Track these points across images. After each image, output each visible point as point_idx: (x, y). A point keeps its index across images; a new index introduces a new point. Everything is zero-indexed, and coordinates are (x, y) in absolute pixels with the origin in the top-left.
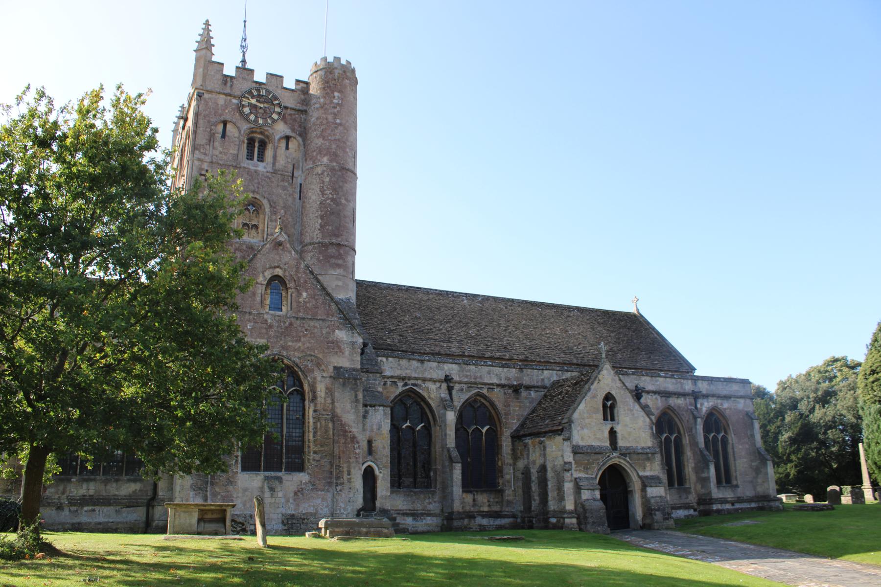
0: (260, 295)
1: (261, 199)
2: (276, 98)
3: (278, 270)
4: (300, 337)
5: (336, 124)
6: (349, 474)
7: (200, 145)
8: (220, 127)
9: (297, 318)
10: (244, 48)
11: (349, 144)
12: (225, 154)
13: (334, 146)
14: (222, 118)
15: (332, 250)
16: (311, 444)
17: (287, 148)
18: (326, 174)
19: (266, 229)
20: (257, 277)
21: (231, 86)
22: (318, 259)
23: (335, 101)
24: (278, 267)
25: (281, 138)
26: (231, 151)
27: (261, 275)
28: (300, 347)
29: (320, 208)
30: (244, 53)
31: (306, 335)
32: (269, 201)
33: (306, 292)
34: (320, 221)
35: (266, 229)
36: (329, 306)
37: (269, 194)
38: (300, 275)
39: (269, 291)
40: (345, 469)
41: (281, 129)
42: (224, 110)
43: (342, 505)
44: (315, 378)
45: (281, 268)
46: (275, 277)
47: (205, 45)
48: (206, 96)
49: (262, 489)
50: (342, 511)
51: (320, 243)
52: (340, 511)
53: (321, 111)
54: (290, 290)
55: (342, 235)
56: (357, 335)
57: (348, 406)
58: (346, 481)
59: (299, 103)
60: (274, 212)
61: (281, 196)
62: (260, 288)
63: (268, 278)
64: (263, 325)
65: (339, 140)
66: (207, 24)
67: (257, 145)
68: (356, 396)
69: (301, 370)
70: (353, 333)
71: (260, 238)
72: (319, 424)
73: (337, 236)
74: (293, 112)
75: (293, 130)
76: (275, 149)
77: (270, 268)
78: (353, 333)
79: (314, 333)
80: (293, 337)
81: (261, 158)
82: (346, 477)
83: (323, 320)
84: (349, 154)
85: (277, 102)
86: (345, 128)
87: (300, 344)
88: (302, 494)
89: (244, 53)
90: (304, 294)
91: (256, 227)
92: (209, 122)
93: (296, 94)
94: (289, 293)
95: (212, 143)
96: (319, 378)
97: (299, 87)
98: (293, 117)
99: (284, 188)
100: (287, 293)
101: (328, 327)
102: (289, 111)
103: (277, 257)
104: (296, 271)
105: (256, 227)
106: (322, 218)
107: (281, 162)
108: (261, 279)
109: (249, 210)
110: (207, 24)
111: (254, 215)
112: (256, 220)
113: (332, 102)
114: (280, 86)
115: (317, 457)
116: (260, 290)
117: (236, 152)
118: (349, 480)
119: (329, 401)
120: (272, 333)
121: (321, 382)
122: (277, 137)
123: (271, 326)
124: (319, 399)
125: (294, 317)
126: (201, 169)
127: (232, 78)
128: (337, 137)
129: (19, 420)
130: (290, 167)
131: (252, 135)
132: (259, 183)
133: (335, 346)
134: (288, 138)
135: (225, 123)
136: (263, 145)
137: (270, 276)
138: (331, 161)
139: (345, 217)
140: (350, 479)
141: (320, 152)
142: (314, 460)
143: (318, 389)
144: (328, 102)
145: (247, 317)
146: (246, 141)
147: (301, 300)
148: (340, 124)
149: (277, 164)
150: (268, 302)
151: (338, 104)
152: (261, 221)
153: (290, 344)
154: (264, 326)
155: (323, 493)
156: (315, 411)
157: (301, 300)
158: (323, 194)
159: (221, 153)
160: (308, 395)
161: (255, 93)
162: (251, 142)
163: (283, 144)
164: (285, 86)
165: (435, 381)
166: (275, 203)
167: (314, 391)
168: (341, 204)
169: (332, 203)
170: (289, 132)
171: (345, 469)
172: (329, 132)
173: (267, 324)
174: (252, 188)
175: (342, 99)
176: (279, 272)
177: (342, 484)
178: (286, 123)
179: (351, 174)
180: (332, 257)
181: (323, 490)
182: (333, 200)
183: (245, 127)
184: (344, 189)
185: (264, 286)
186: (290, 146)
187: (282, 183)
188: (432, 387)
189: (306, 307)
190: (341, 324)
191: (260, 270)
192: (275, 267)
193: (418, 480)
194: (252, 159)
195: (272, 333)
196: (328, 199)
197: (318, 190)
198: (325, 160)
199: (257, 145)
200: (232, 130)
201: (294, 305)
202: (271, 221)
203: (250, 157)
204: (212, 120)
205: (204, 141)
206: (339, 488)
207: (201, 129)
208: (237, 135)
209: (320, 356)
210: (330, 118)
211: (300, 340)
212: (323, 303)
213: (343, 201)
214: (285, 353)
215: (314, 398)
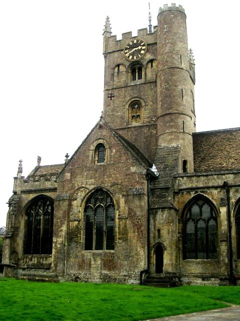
3: (100, 140)
8: (116, 69)
10: (150, 20)
13: (166, 57)
16: (117, 234)
17: (152, 66)
20: (90, 147)
25: (148, 62)
45: (101, 139)
47: (107, 32)
55: (172, 108)
63: (95, 146)
65: (168, 52)
66: (108, 18)
67: (137, 71)
69: (111, 194)
73: (169, 109)
81: (140, 77)
84: (176, 58)
91: (139, 116)
105: (139, 116)
107: (149, 75)
110: (108, 18)
115: (121, 241)
116: (91, 153)
134: (151, 61)
135: (118, 66)
136: (140, 70)
143: (121, 203)
150: (97, 159)
159: (117, 82)
160: (116, 207)
162: (133, 72)
163: (150, 65)
165: (216, 188)
167: (118, 203)
176: (101, 141)
183: (127, 64)
186: (154, 65)
188: (215, 192)
199: (137, 71)
202: (145, 111)
203: (134, 79)
208: (125, 70)
215: (119, 207)
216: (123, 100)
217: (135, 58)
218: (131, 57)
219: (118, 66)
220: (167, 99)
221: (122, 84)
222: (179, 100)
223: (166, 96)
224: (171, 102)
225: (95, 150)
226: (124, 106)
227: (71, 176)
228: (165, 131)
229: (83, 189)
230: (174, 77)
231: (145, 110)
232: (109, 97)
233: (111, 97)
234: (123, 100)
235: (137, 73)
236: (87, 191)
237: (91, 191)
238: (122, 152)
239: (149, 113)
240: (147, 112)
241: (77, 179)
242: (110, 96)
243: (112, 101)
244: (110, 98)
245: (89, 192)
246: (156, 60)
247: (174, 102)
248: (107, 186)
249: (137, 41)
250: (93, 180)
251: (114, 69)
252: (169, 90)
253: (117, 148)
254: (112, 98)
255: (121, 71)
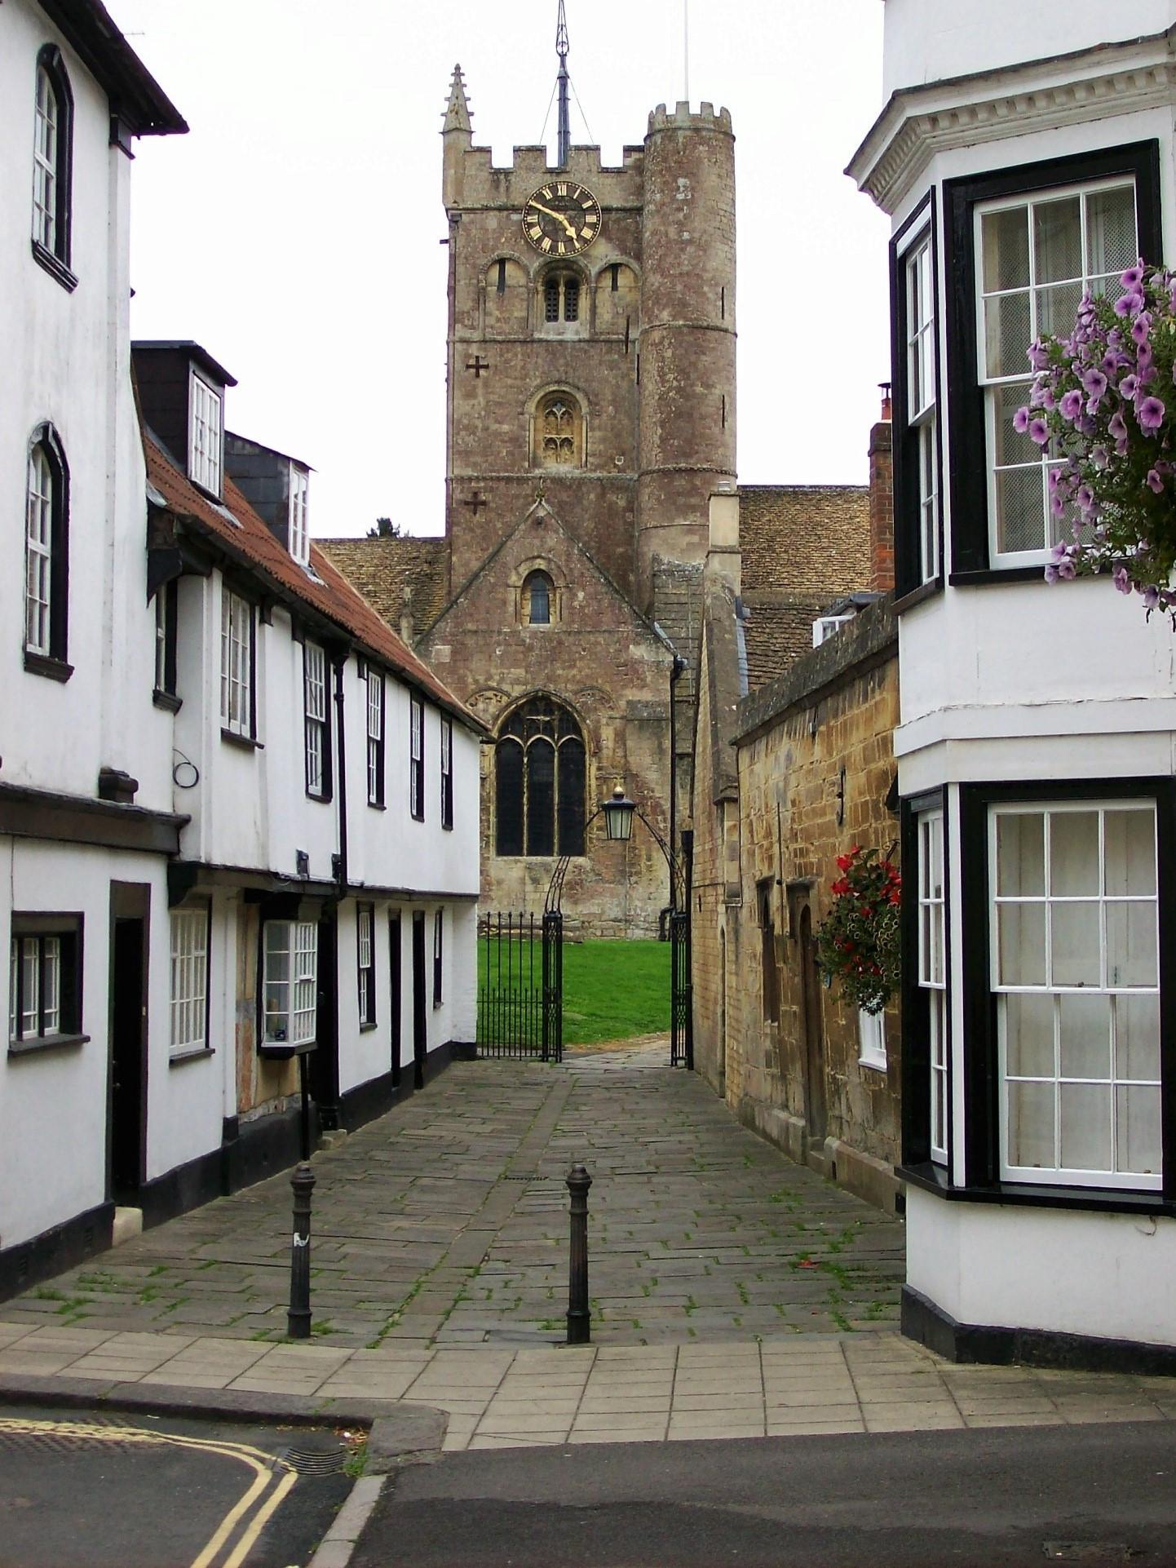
0: (513, 604)
1: (574, 392)
2: (586, 196)
3: (539, 561)
4: (575, 661)
5: (682, 242)
6: (649, 859)
7: (463, 313)
8: (494, 273)
9: (569, 633)
11: (707, 276)
12: (507, 320)
13: (679, 287)
14: (495, 256)
15: (681, 482)
17: (615, 287)
18: (666, 343)
19: (584, 445)
20: (507, 576)
21: (508, 188)
22: (658, 499)
23: (680, 197)
24: (539, 557)
26: (516, 314)
27: (514, 572)
28: (574, 676)
29: (659, 406)
30: (563, 56)
31: (584, 656)
32: (586, 395)
33: (584, 590)
34: (660, 431)
35: (584, 445)
36: (620, 608)
37: (586, 381)
38: (573, 566)
39: (528, 595)
40: (644, 852)
41: (604, 252)
42: (499, 238)
43: (639, 904)
44: (598, 721)
45: (543, 558)
46: (536, 574)
48: (465, 218)
49: (523, 882)
50: (639, 911)
51: (659, 470)
52: (635, 910)
53: (657, 220)
54: (558, 591)
56: (664, 650)
57: (648, 760)
58: (644, 870)
59: (633, 194)
60: (594, 414)
61: (607, 381)
62: (514, 592)
63: (524, 575)
64: (518, 648)
65: (688, 274)
66: (458, 72)
67: (562, 289)
68: (660, 744)
70: (658, 648)
71: (575, 462)
72: (605, 787)
73: (687, 455)
74: (620, 215)
75: (624, 251)
76: (594, 292)
77: (527, 560)
78: (658, 648)
79: (596, 654)
80: (564, 662)
81: (572, 316)
82: (643, 862)
83: (610, 632)
84: (710, 295)
85: (590, 203)
86: (699, 247)
87: (574, 672)
88: (581, 887)
89: (563, 56)
90: (581, 595)
92: (474, 266)
93: (626, 177)
94: (558, 595)
95: (482, 306)
96: (604, 721)
97: (630, 161)
98: (623, 224)
99: (612, 366)
100: (555, 595)
101: (618, 641)
102: (614, 215)
103: (537, 542)
104: (567, 561)
105: (567, 442)
106: (663, 424)
107: (605, 314)
108: (513, 579)
109: (555, 414)
110: (458, 72)
111: (565, 420)
112: (568, 429)
113: (674, 199)
114: (594, 169)
116: (512, 595)
117: (524, 314)
118: (649, 868)
119: (620, 753)
120: (532, 659)
121: (608, 724)
122: (594, 270)
123: (530, 648)
124: (605, 751)
125: (565, 632)
126: (468, 356)
127: (506, 172)
128: (685, 269)
129: (1071, 534)
130: (622, 322)
131: (552, 274)
132: (567, 365)
133: (631, 672)
134: (614, 268)
135: (502, 262)
136: (573, 286)
137: (527, 572)
138: (674, 318)
139: (703, 417)
140: (651, 866)
141: (657, 302)
142: (598, 839)
143: (604, 737)
144: (667, 200)
145: (495, 638)
146: (541, 288)
147: (576, 604)
148: (690, 242)
149: (597, 321)
150: (528, 610)
151: (685, 201)
152: (576, 430)
153: (560, 672)
154: (521, 648)
155: (612, 885)
156: (599, 769)
157: (576, 604)
158: (663, 381)
159: (498, 320)
160: (589, 747)
161: (549, 195)
162: (551, 286)
163: (607, 282)
164: (604, 164)
166: (596, 395)
167: (597, 740)
168: (694, 395)
169: (677, 397)
170: (615, 257)
171: (644, 852)
172: (670, 260)
173: (524, 645)
174: (556, 375)
175: (693, 189)
176: (541, 564)
177: (638, 873)
178: (609, 239)
179: (716, 334)
180: (679, 494)
181: (613, 883)
182: (679, 390)
183: (535, 264)
184: (700, 366)
185: (519, 590)
187: (607, 358)
189: (585, 614)
190: (637, 634)
191: (512, 565)
192: (535, 558)
193: (36, 1012)
194: (556, 318)
195: (532, 659)
196: (670, 389)
197: (656, 373)
198: (665, 315)
199: (562, 289)
200: (513, 274)
201: (565, 613)
202: (593, 429)
204: (478, 262)
205: (470, 304)
206: (633, 879)
207: (462, 282)
208: (523, 281)
209: (608, 688)
210: (672, 232)
211: (575, 666)
212: (611, 605)
213: (699, 389)
214: (551, 687)
216: (518, 382)
217: (561, 248)
218: (547, 243)
219: (502, 262)
220: (681, 423)
221: (512, 330)
222: (716, 430)
223: (679, 415)
224: (693, 434)
225: (524, 589)
226: (524, 403)
227: (454, 653)
228: (673, 520)
229: (490, 694)
230: (704, 358)
231: (590, 428)
232: (468, 367)
233: (478, 367)
234: (518, 382)
235: (562, 299)
236: (505, 699)
237: (518, 698)
238: (606, 603)
239: (603, 440)
240: (598, 434)
241: (473, 665)
242: (472, 362)
243: (479, 382)
244: (473, 371)
245: (508, 705)
246: (627, 266)
247: (702, 435)
248: (564, 691)
249: (571, 188)
250: (520, 672)
251: (486, 272)
252: (687, 397)
253: (590, 589)
254: (482, 372)
255: (509, 281)
